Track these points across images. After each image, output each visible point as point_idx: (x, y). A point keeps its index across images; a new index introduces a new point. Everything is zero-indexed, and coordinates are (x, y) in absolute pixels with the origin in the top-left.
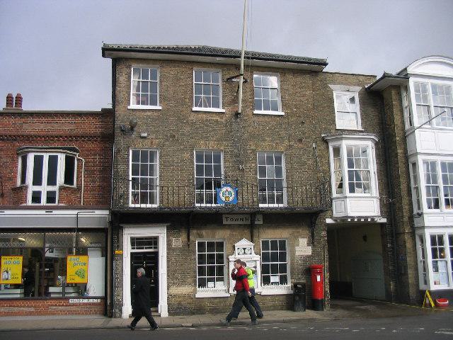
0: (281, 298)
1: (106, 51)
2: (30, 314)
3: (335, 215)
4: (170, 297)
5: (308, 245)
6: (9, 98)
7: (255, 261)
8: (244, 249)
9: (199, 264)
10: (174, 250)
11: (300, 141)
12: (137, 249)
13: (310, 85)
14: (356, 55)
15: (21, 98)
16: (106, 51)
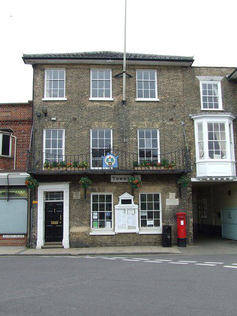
1: (27, 59)
5: (176, 197)
7: (135, 209)
10: (75, 200)
11: (172, 120)
16: (27, 59)
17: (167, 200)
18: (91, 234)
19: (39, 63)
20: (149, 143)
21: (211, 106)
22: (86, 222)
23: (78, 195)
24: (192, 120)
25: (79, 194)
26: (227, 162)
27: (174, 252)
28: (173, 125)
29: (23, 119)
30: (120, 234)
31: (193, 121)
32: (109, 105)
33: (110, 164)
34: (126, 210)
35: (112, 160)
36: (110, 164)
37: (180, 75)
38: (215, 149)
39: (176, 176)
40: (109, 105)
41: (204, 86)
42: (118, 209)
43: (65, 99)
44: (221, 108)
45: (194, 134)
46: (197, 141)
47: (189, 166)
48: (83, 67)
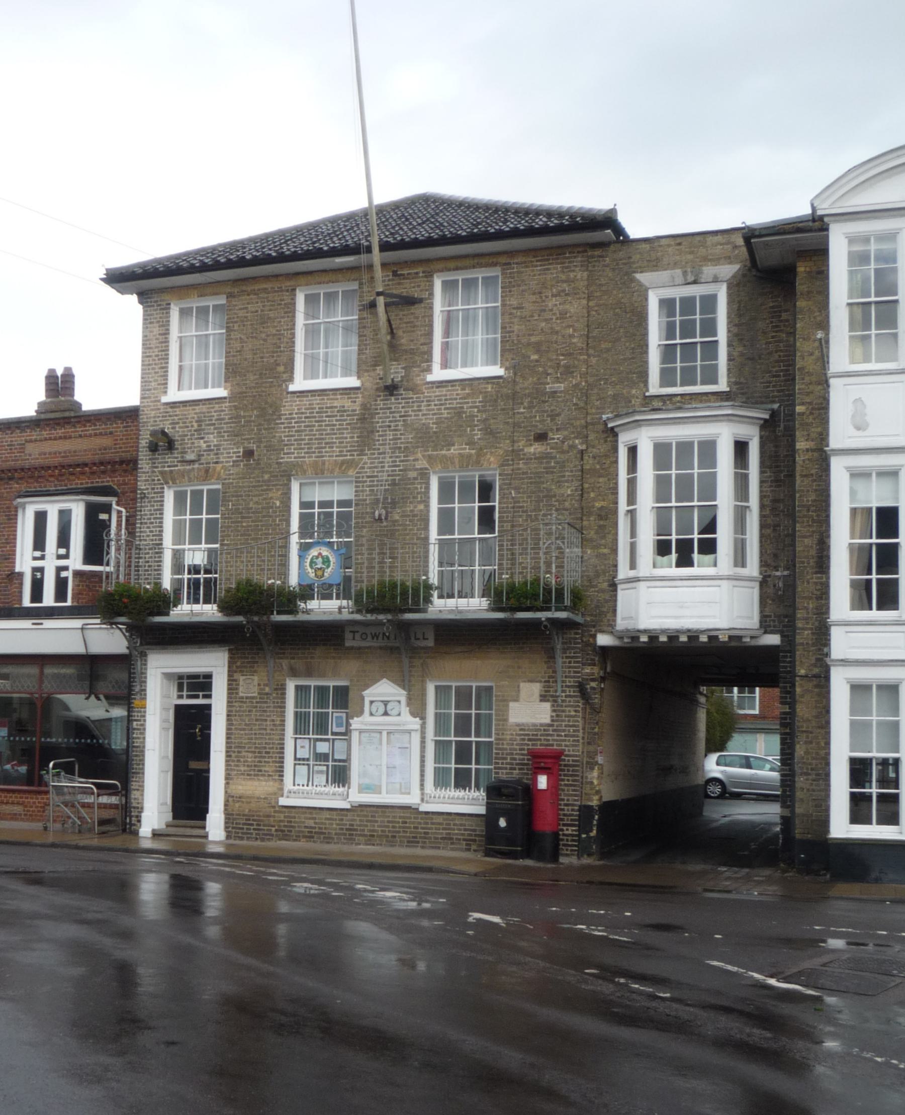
0: (468, 823)
1: (119, 279)
2: (14, 817)
3: (621, 624)
4: (230, 799)
5: (543, 698)
6: (51, 378)
7: (409, 732)
8: (386, 703)
9: (478, 688)
10: (242, 700)
11: (541, 437)
12: (189, 697)
13: (582, 284)
14: (683, 191)
15: (73, 376)
16: (119, 279)
17: (511, 704)
18: (283, 801)
19: (150, 282)
20: (470, 520)
21: (689, 379)
22: (270, 768)
23: (250, 686)
24: (613, 433)
25: (256, 683)
26: (720, 578)
27: (111, 829)
28: (547, 457)
29: (81, 453)
30: (362, 807)
31: (616, 435)
32: (347, 404)
33: (320, 573)
34: (385, 734)
35: (326, 561)
36: (320, 573)
37: (580, 275)
38: (685, 548)
39: (536, 622)
40: (347, 404)
41: (667, 305)
42: (361, 732)
43: (222, 392)
44: (722, 385)
45: (616, 484)
46: (623, 506)
47: (594, 597)
48: (276, 285)
